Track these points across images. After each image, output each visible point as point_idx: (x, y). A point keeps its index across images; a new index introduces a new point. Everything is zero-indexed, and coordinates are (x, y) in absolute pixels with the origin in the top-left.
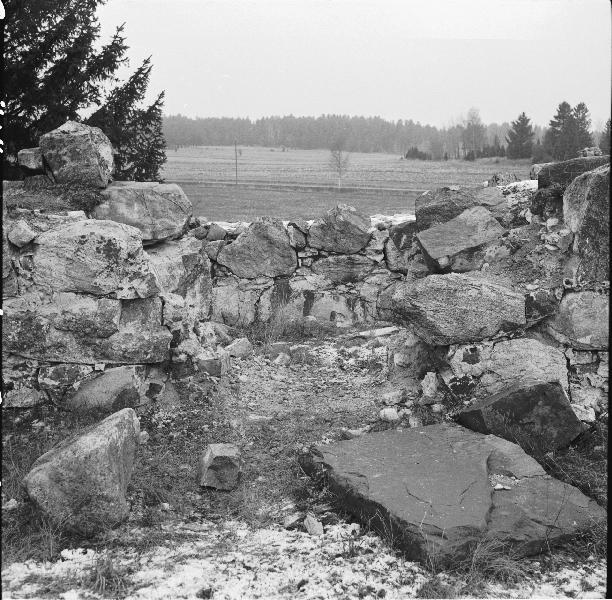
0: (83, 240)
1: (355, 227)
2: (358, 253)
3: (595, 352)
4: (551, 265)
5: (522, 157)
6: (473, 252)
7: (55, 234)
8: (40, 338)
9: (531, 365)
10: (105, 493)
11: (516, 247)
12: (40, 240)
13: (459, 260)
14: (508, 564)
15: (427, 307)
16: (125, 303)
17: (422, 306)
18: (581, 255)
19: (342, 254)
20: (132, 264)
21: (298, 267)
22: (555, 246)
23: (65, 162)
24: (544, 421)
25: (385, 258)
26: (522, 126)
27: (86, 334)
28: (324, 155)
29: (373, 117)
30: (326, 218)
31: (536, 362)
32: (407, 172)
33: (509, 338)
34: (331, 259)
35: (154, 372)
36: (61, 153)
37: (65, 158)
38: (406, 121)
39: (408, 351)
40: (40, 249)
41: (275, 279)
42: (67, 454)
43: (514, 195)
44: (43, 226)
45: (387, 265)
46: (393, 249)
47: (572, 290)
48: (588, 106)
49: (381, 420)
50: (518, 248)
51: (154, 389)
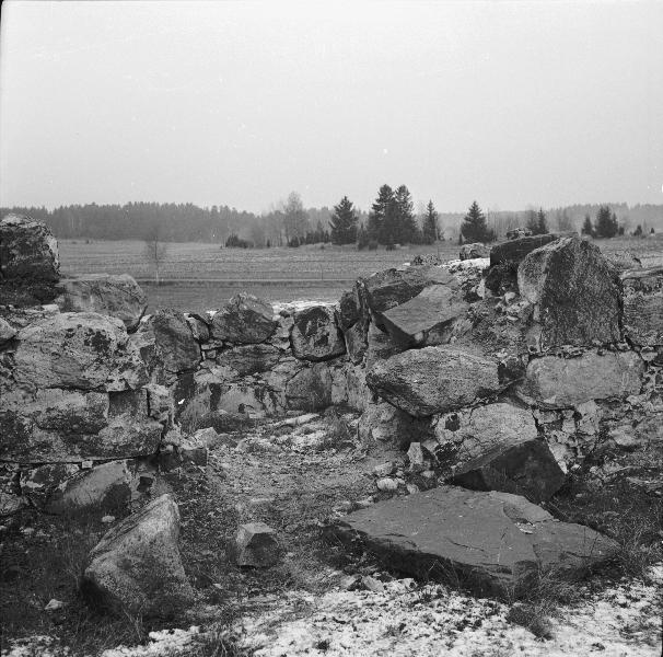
0: (70, 334)
1: (259, 315)
2: (264, 342)
3: (559, 411)
4: (513, 334)
5: (348, 243)
6: (444, 327)
7: (38, 329)
8: (24, 438)
9: (504, 429)
10: (175, 574)
11: (477, 321)
12: (23, 335)
13: (431, 335)
14: (565, 588)
15: (413, 380)
16: (113, 395)
17: (407, 379)
18: (542, 322)
19: (248, 344)
20: (121, 355)
21: (202, 360)
22: (516, 316)
23: (14, 255)
24: (534, 474)
25: (292, 346)
26: (345, 210)
27: (73, 431)
28: (140, 246)
29: (185, 204)
30: (229, 307)
31: (511, 424)
32: (229, 262)
33: (484, 404)
34: (236, 350)
35: (142, 467)
36: (9, 246)
37: (14, 251)
38: (221, 207)
39: (384, 425)
40: (23, 344)
41: (178, 374)
42: (130, 539)
43: (461, 273)
44: (22, 321)
45: (294, 353)
46: (299, 336)
47: (536, 356)
48: (409, 188)
49: (380, 490)
50: (479, 320)
51: (145, 483)
